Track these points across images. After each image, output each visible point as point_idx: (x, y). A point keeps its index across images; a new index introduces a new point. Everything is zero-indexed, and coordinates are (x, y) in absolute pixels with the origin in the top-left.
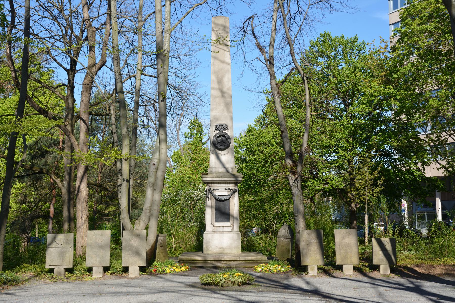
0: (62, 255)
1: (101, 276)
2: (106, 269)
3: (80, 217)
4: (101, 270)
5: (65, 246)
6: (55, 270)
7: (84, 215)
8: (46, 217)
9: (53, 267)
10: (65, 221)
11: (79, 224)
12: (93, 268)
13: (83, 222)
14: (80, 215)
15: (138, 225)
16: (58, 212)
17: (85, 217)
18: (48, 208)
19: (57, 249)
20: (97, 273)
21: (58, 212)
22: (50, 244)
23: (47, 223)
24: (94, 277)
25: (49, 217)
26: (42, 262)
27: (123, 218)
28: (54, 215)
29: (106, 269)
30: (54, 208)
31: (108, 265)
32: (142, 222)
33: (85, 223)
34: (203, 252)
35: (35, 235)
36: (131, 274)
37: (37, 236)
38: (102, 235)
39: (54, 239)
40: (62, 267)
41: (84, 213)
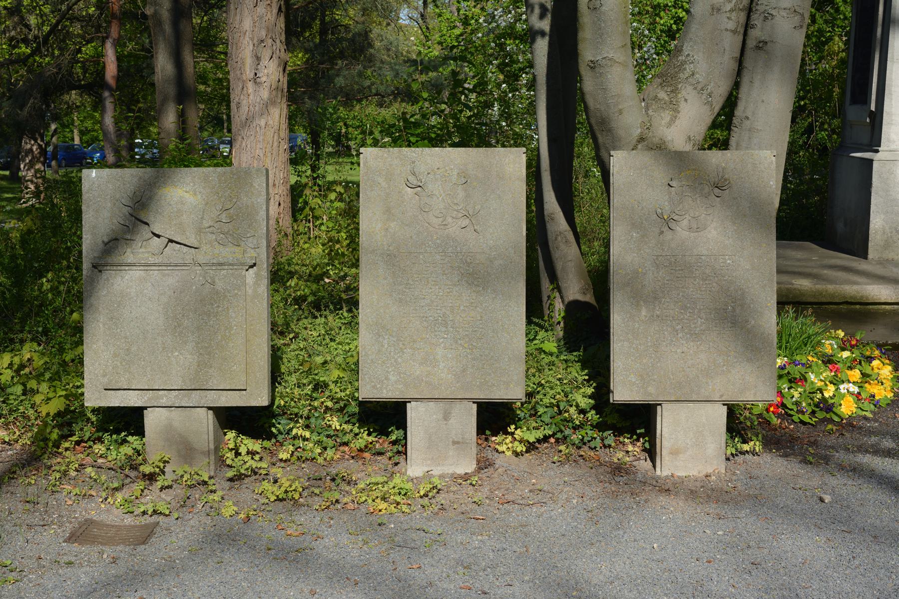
0: (199, 313)
1: (469, 467)
2: (494, 418)
3: (249, 73)
4: (469, 418)
5: (209, 252)
6: (151, 420)
7: (265, 62)
8: (95, 86)
9: (132, 400)
10: (165, 101)
11: (244, 109)
12: (412, 411)
13: (265, 94)
14: (249, 61)
15: (666, 116)
16: (136, 69)
17: (271, 72)
18: (98, 57)
19: (155, 274)
20: (438, 445)
21: (136, 69)
22: (113, 244)
23: (98, 105)
24: (415, 467)
25: (104, 85)
26: (63, 337)
27: (593, 66)
28: (118, 79)
29: (494, 418)
30: (119, 59)
31: (511, 390)
32: (687, 92)
33: (272, 102)
34: (866, 258)
35: (73, 139)
36: (675, 452)
37: (77, 141)
38: (466, 180)
39: (137, 214)
40: (195, 398)
41: (266, 54)
